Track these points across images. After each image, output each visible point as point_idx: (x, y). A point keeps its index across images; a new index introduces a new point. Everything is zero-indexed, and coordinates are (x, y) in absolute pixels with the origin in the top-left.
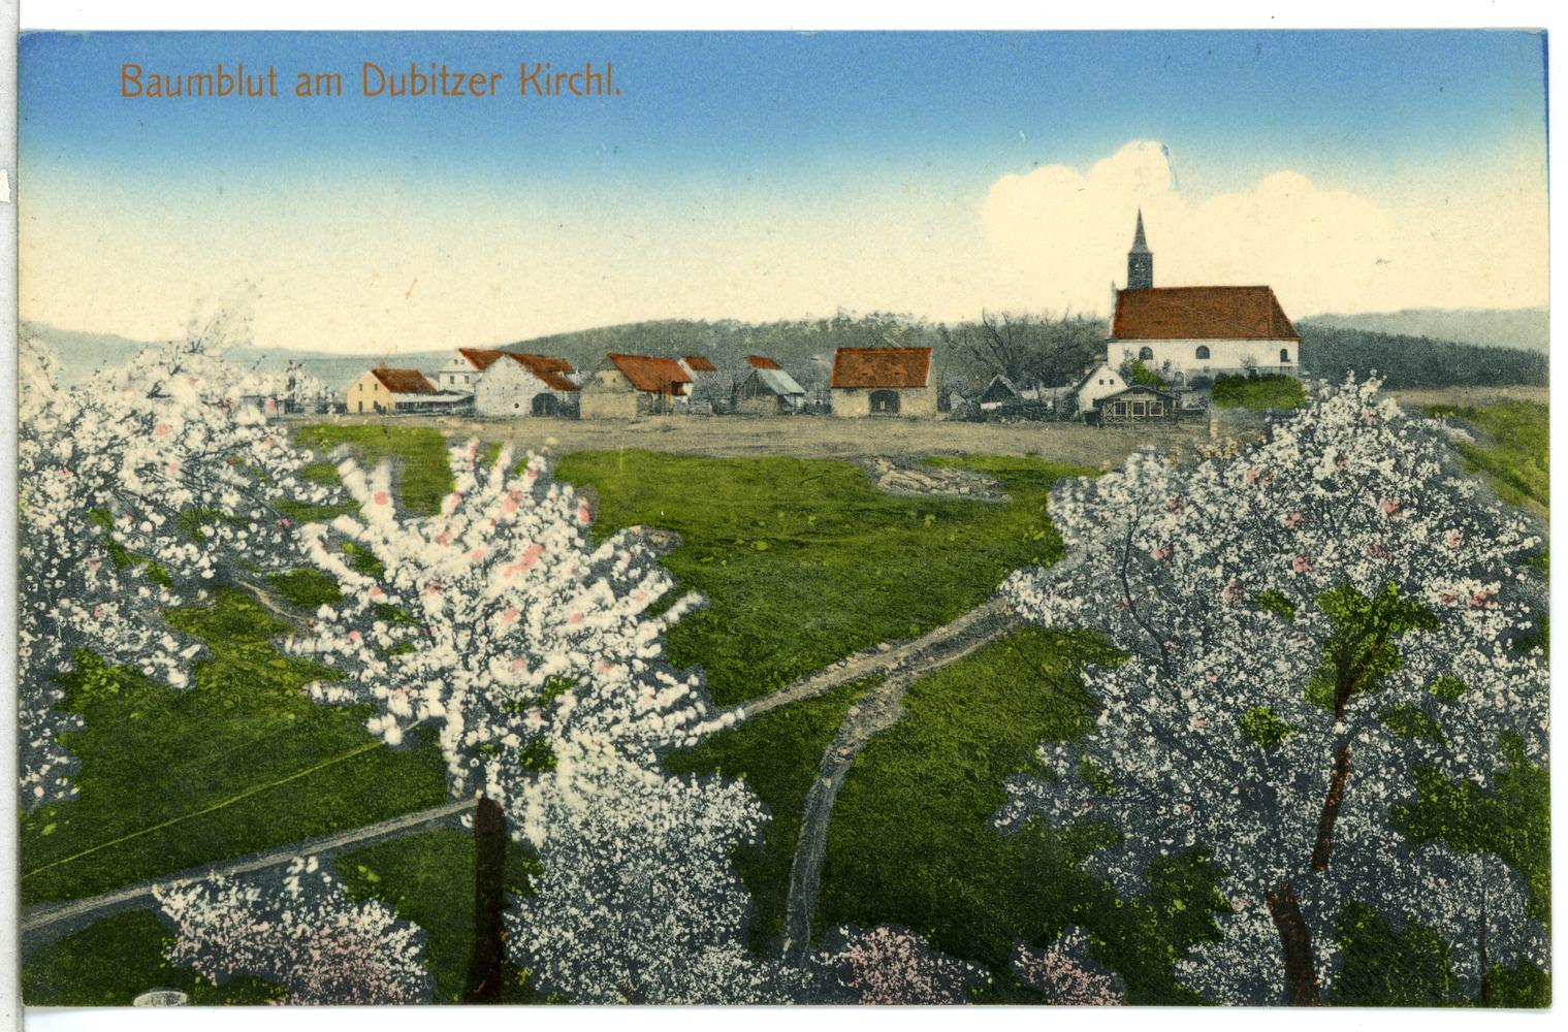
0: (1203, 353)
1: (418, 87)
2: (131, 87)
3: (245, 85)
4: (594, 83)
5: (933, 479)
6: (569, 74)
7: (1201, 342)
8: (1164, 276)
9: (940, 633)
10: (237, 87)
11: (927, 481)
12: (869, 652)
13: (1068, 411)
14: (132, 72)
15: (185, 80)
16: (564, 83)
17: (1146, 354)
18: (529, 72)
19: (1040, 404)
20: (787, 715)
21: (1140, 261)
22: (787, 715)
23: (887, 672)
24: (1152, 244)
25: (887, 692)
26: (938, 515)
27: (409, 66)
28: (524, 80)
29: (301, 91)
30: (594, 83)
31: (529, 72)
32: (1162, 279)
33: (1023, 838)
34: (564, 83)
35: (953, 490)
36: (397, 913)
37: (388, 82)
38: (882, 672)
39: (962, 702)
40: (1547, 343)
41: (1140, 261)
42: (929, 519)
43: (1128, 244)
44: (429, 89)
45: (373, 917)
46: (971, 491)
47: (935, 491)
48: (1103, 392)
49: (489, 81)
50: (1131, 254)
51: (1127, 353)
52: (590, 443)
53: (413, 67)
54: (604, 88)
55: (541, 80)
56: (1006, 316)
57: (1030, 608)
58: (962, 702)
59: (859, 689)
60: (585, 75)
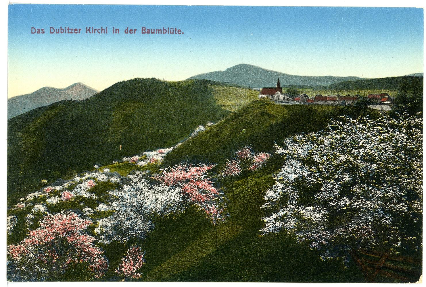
2: (144, 32)
3: (170, 31)
4: (103, 31)
6: (97, 29)
10: (167, 32)
14: (144, 29)
15: (155, 30)
16: (96, 31)
18: (88, 28)
27: (86, 28)
28: (87, 30)
29: (38, 32)
30: (103, 31)
31: (88, 28)
34: (96, 31)
36: (350, 179)
37: (55, 31)
40: (94, 91)
44: (65, 32)
49: (78, 30)
52: (78, 179)
53: (61, 27)
54: (105, 32)
55: (91, 30)
56: (158, 79)
57: (161, 192)
60: (101, 30)
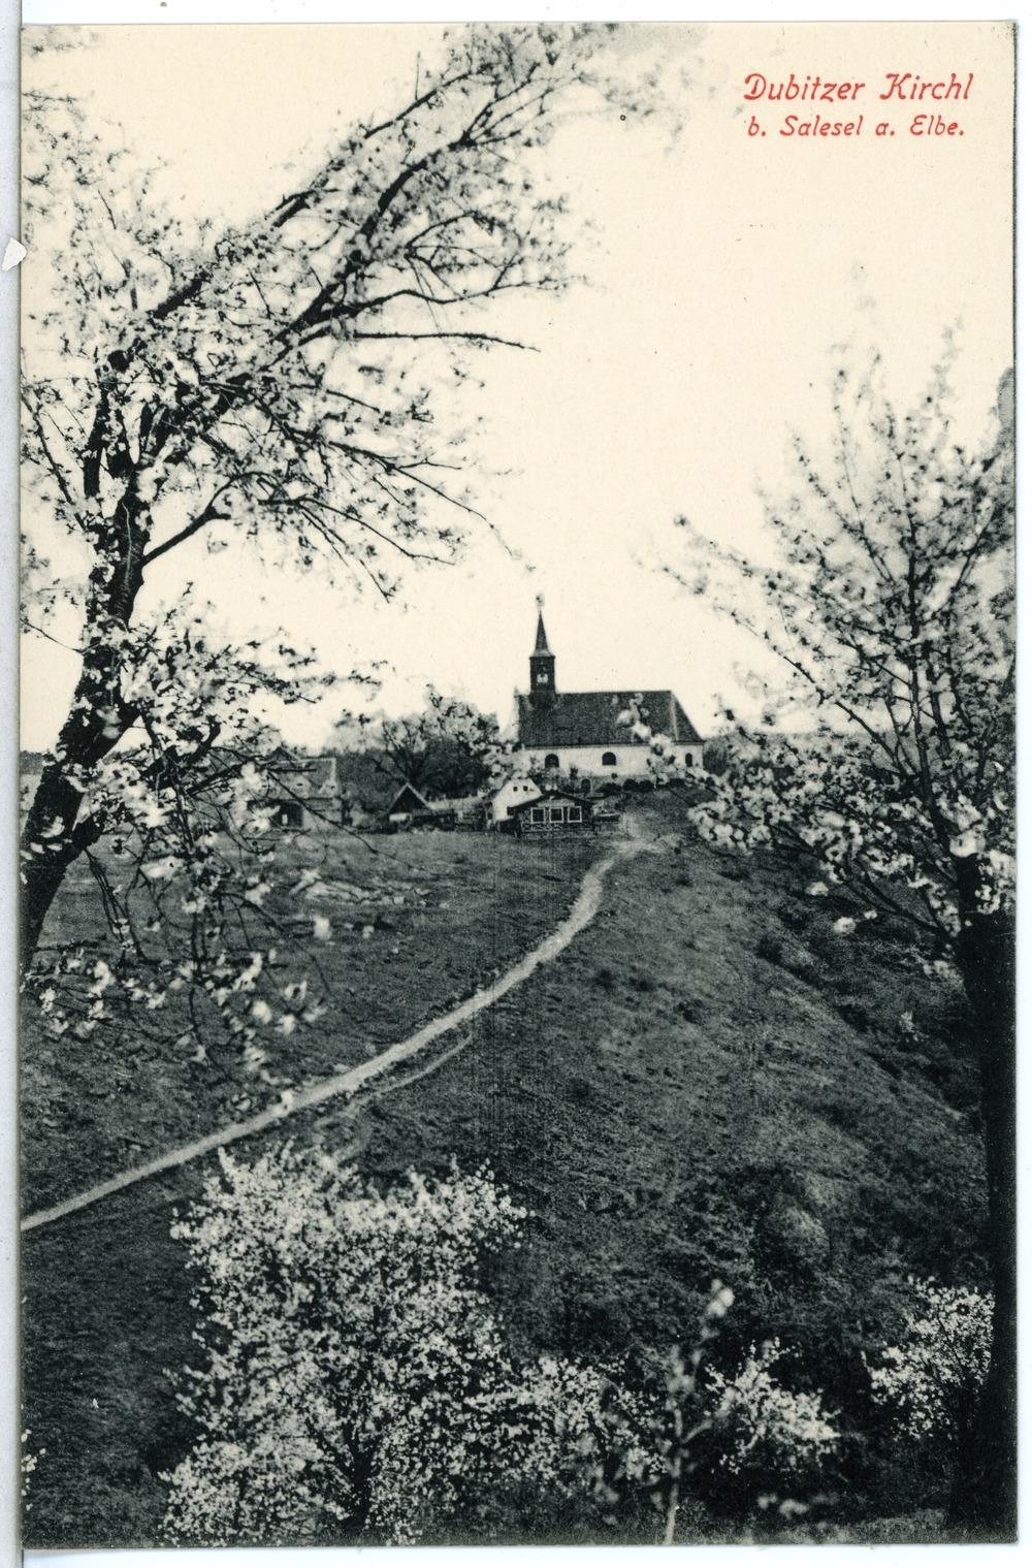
0: (609, 759)
1: (792, 93)
5: (364, 889)
7: (606, 750)
8: (567, 681)
9: (396, 1052)
11: (358, 892)
12: (325, 1074)
13: (479, 820)
17: (552, 761)
19: (452, 814)
20: (247, 1148)
21: (542, 664)
22: (247, 1148)
23: (348, 1096)
24: (554, 646)
25: (352, 1117)
26: (376, 926)
32: (567, 681)
33: (851, 1259)
35: (386, 900)
38: (344, 1095)
39: (431, 1123)
41: (542, 664)
42: (368, 930)
43: (529, 648)
45: (808, 1404)
46: (405, 901)
47: (367, 902)
48: (519, 798)
50: (532, 659)
51: (533, 760)
58: (431, 1123)
59: (321, 1115)
